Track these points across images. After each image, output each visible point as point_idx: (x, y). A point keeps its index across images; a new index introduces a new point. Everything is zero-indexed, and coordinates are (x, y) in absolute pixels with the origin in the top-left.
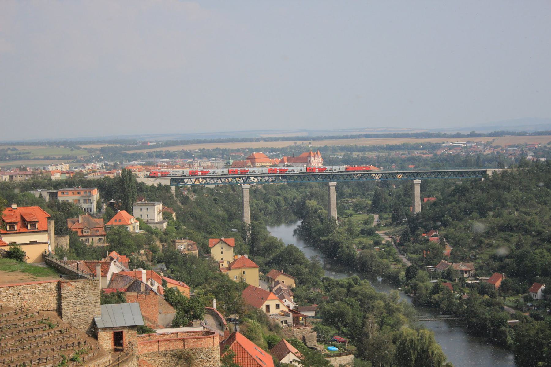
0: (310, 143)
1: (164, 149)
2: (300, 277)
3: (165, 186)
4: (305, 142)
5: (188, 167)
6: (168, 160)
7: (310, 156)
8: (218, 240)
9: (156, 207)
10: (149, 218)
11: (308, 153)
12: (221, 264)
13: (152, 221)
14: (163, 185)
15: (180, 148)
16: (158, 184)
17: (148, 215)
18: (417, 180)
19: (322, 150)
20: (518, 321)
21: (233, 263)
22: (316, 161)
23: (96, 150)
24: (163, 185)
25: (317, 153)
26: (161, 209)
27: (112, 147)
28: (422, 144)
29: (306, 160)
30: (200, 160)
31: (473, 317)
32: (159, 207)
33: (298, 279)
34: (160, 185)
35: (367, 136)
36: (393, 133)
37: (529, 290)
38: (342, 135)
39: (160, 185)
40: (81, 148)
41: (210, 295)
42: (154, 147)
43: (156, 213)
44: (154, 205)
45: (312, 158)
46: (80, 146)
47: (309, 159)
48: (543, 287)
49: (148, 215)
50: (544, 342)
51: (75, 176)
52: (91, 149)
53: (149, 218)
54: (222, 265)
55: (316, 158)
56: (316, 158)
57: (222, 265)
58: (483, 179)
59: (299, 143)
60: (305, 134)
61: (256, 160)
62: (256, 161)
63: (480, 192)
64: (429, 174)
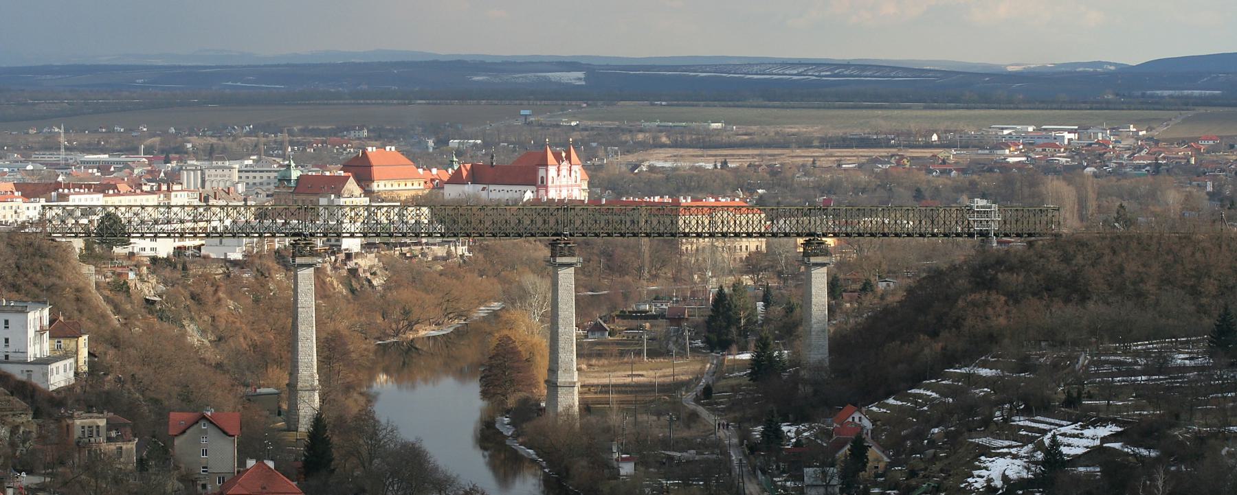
5: (151, 192)
10: (11, 349)
13: (20, 357)
17: (7, 340)
20: (934, 395)
22: (564, 181)
25: (568, 158)
26: (46, 322)
32: (38, 317)
41: (752, 340)
43: (31, 333)
44: (24, 311)
45: (552, 171)
47: (541, 172)
49: (7, 340)
50: (976, 297)
51: (1007, 252)
53: (11, 349)
55: (564, 172)
61: (376, 171)
63: (168, 269)
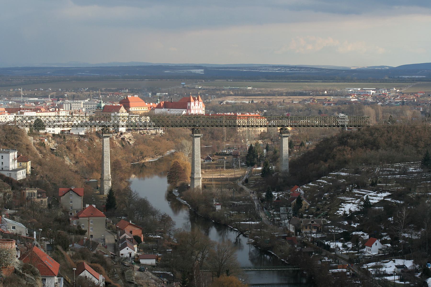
6: (36, 99)
9: (11, 154)
10: (4, 166)
17: (2, 163)
20: (325, 182)
21: (82, 211)
22: (196, 107)
25: (198, 99)
26: (16, 157)
30: (72, 101)
32: (13, 155)
43: (11, 160)
44: (8, 153)
45: (192, 104)
47: (189, 104)
49: (2, 163)
50: (340, 148)
53: (4, 166)
55: (197, 104)
56: (197, 104)
58: (296, 246)
61: (131, 104)
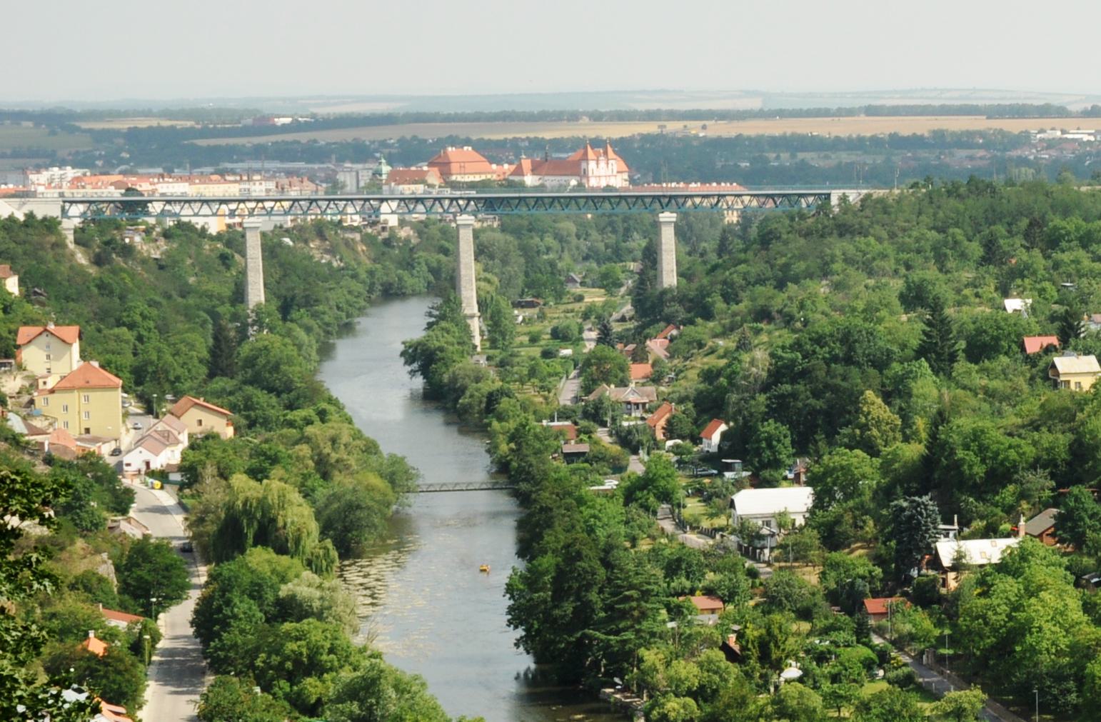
0: (704, 127)
1: (304, 137)
2: (252, 414)
3: (45, 219)
4: (691, 124)
7: (585, 158)
8: (40, 329)
11: (581, 152)
12: (41, 381)
14: (39, 216)
15: (348, 135)
16: (26, 215)
18: (667, 214)
19: (624, 149)
23: (117, 133)
24: (39, 216)
25: (606, 153)
27: (173, 127)
28: (981, 134)
29: (576, 168)
31: (524, 480)
33: (247, 417)
34: (30, 216)
35: (872, 111)
36: (937, 103)
37: (702, 435)
38: (835, 107)
39: (30, 216)
40: (79, 129)
42: (285, 129)
45: (592, 165)
46: (77, 124)
47: (584, 165)
48: (723, 427)
52: (104, 131)
54: (45, 383)
55: (602, 164)
56: (602, 164)
57: (45, 383)
59: (673, 127)
60: (755, 104)
62: (453, 171)
64: (648, 201)
